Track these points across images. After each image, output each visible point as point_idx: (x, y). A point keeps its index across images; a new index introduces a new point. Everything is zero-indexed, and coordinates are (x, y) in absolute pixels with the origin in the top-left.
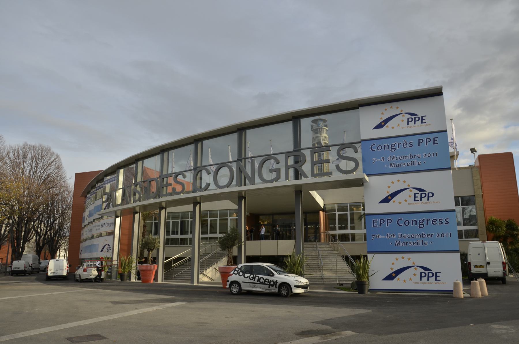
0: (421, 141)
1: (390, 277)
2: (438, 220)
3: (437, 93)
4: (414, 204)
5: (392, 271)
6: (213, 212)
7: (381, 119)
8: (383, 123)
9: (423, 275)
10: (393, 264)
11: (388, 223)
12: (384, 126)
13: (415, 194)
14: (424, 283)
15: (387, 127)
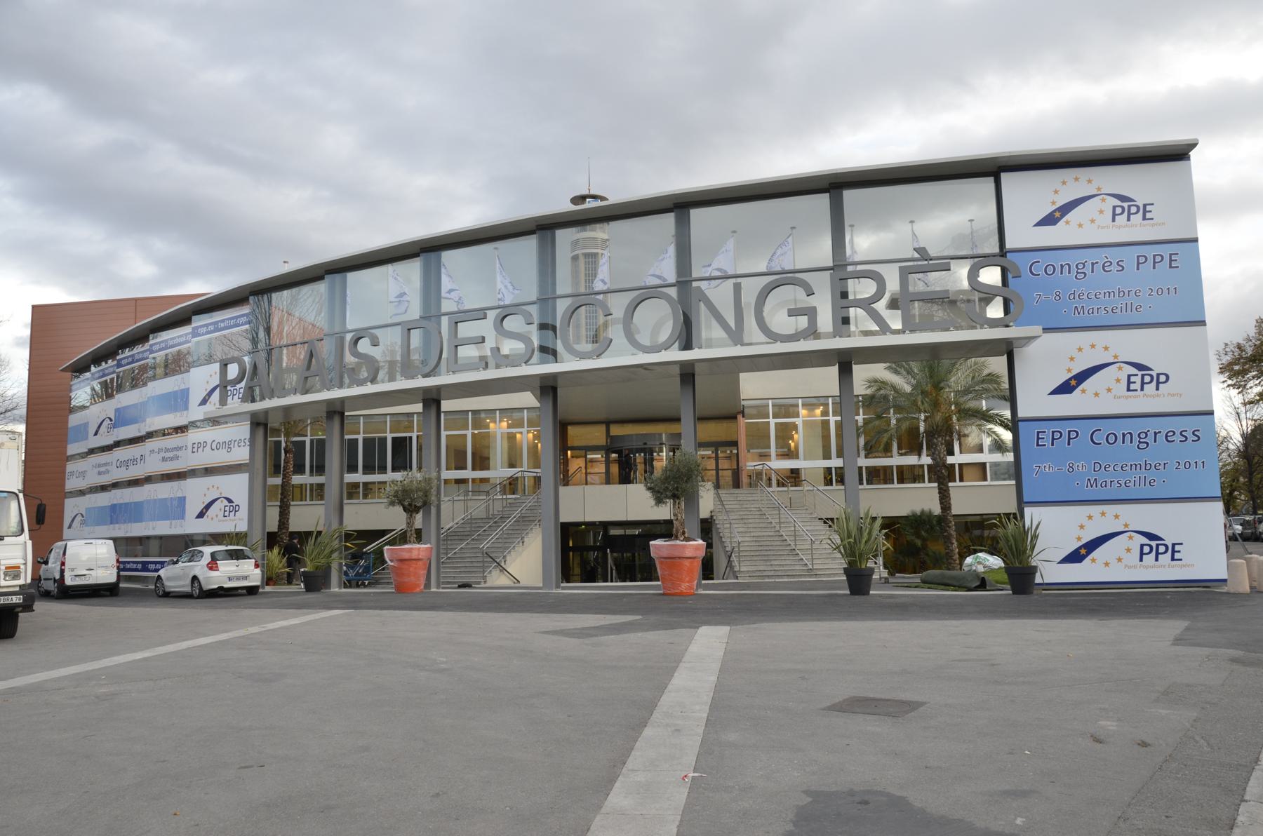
0: (1142, 260)
1: (1075, 557)
2: (1178, 433)
3: (1178, 154)
4: (1127, 397)
5: (1054, 207)
6: (614, 532)
7: (1053, 203)
8: (1057, 214)
9: (1119, 210)
10: (1082, 527)
11: (1069, 439)
12: (1058, 220)
13: (1129, 376)
14: (1147, 567)
15: (1093, 560)
